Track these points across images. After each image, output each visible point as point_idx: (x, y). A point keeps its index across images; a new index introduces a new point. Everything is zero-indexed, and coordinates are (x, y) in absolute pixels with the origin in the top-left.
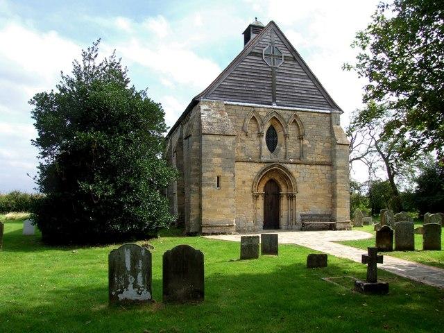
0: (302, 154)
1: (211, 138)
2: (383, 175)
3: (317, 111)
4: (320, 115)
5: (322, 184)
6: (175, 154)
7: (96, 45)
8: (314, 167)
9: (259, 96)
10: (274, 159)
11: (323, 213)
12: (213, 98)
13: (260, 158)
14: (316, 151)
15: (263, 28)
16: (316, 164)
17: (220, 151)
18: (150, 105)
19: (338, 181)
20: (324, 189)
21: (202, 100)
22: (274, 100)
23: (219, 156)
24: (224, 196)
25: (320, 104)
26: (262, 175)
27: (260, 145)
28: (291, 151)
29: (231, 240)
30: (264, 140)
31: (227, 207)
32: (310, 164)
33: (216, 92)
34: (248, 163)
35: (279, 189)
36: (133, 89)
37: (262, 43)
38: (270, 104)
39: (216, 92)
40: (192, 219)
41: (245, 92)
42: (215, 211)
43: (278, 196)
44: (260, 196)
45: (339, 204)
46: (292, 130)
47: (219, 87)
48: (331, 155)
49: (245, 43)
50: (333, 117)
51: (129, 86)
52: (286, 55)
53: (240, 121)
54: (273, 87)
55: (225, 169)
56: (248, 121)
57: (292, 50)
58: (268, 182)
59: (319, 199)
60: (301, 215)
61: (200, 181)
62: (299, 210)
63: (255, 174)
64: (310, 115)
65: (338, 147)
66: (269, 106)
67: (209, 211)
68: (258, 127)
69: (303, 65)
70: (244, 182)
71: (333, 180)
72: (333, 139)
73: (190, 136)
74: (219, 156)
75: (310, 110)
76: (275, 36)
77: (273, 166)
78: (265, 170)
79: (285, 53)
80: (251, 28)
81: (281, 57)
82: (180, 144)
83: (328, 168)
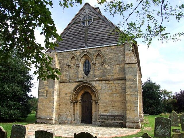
0: (104, 73)
5: (118, 93)
7: (171, 14)
8: (112, 82)
14: (114, 71)
20: (120, 97)
26: (77, 91)
32: (109, 80)
34: (69, 83)
41: (73, 45)
42: (44, 110)
46: (98, 61)
52: (94, 18)
55: (49, 87)
59: (116, 104)
60: (100, 115)
65: (127, 66)
66: (83, 49)
67: (41, 110)
77: (84, 83)
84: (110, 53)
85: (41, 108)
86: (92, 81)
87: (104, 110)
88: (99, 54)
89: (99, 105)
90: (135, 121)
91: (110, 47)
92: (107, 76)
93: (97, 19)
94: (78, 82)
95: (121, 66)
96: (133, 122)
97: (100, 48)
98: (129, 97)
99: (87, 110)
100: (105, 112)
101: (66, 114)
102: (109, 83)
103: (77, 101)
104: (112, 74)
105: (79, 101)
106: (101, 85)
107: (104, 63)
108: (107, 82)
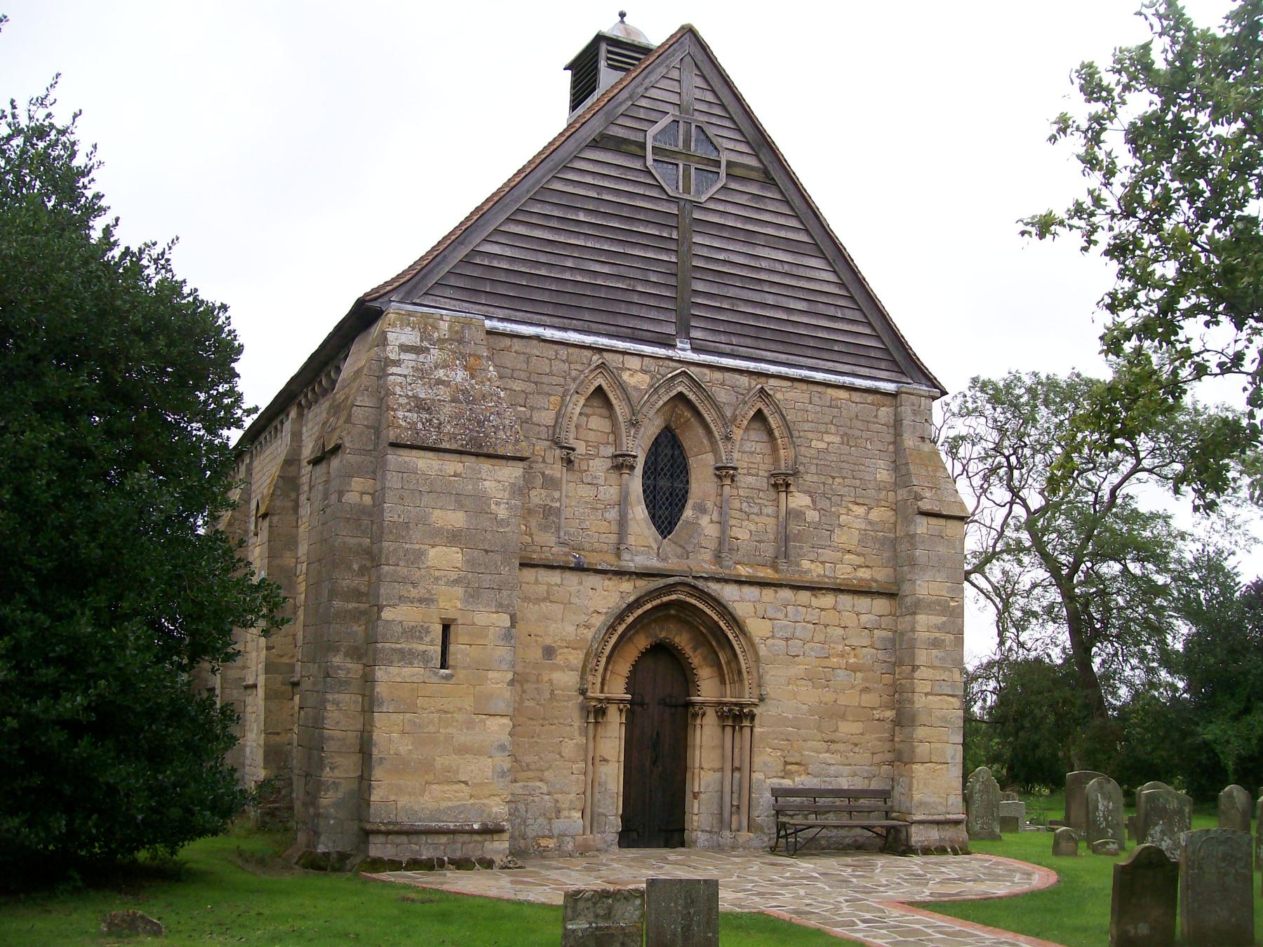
0: (786, 544)
1: (424, 463)
2: (1049, 641)
3: (847, 380)
4: (856, 396)
5: (854, 669)
6: (266, 524)
8: (827, 600)
9: (623, 309)
10: (673, 564)
11: (860, 784)
12: (442, 302)
13: (618, 556)
14: (840, 537)
15: (646, 51)
16: (838, 590)
17: (456, 519)
18: (178, 309)
19: (922, 657)
20: (866, 690)
21: (394, 309)
22: (684, 330)
23: (454, 538)
24: (468, 703)
25: (857, 356)
26: (628, 623)
27: (623, 502)
28: (742, 532)
29: (493, 892)
30: (636, 484)
31: (479, 752)
32: (814, 589)
33: (453, 281)
34: (568, 575)
35: (687, 679)
36: (108, 240)
37: (643, 103)
38: (667, 343)
39: (453, 281)
40: (327, 799)
42: (427, 766)
43: (683, 712)
44: (613, 711)
45: (922, 750)
47: (466, 261)
48: (896, 556)
49: (575, 105)
50: (906, 411)
51: (97, 226)
53: (540, 401)
54: (680, 276)
55: (474, 594)
56: (576, 405)
57: (761, 142)
58: (644, 654)
59: (848, 728)
60: (777, 793)
61: (371, 640)
62: (767, 774)
63: (598, 621)
64: (820, 402)
65: (923, 526)
68: (615, 430)
69: (797, 201)
70: (549, 652)
71: (899, 654)
72: (902, 494)
73: (337, 448)
74: (454, 538)
75: (819, 376)
76: (699, 82)
77: (669, 589)
78: (631, 607)
79: (732, 150)
80: (604, 47)
81: (717, 163)
82: (288, 482)
83: (881, 605)
84: (822, 428)
85: (403, 749)
86: (719, 580)
87: (786, 763)
88: (759, 416)
89: (757, 730)
90: (948, 816)
91: (820, 389)
92: (806, 564)
93: (754, 175)
94: (631, 574)
95: (875, 515)
96: (938, 823)
97: (772, 382)
98: (927, 694)
99: (654, 763)
100: (787, 774)
101: (545, 789)
102: (816, 602)
103: (609, 700)
104: (827, 554)
105: (622, 701)
106: (770, 614)
107: (791, 480)
108: (804, 596)
